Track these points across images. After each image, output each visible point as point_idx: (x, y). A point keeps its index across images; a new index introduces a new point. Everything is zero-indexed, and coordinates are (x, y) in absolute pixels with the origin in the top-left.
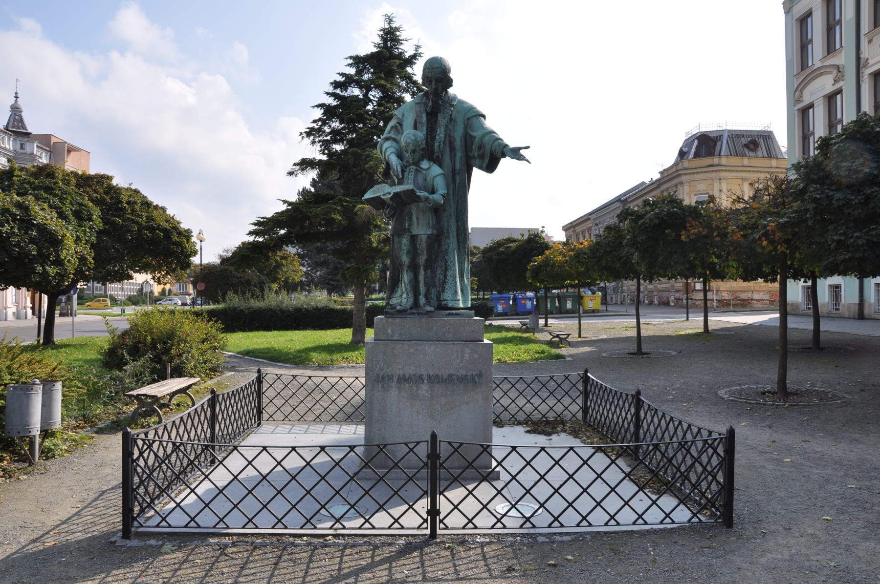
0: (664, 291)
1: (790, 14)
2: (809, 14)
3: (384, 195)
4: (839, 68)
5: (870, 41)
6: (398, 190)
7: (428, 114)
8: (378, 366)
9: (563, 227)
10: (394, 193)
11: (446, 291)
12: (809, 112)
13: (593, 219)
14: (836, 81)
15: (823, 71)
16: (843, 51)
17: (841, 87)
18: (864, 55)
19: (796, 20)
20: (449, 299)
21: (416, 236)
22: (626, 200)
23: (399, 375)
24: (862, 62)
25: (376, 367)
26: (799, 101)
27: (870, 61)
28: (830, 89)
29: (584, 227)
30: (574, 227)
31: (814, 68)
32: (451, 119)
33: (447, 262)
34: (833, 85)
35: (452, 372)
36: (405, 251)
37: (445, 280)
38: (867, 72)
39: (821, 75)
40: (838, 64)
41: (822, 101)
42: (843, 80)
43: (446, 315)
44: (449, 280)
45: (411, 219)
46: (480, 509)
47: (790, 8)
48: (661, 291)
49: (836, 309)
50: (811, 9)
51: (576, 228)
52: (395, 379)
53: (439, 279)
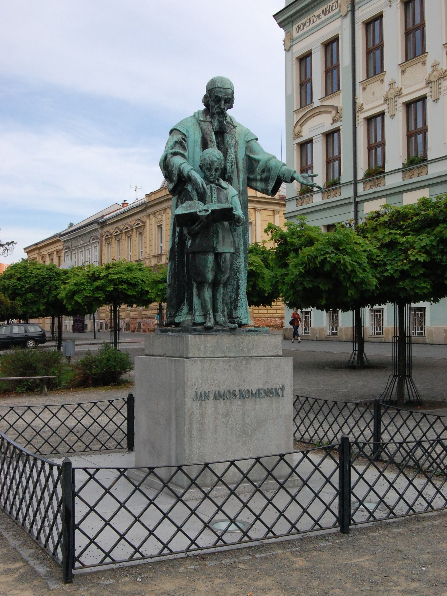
0: (149, 318)
1: (290, 52)
2: (309, 55)
3: (200, 211)
4: (337, 109)
5: (364, 89)
6: (216, 208)
7: (216, 133)
8: (196, 384)
9: (25, 249)
10: (212, 211)
11: (238, 308)
12: (307, 146)
13: (64, 241)
14: (334, 121)
15: (322, 109)
16: (341, 94)
17: (340, 127)
18: (360, 100)
19: (296, 58)
20: (242, 317)
21: (221, 254)
22: (104, 222)
23: (215, 392)
24: (358, 106)
25: (195, 384)
26: (298, 135)
27: (364, 106)
28: (328, 127)
29: (52, 249)
30: (39, 249)
31: (314, 107)
32: (236, 141)
33: (239, 280)
34: (332, 124)
35: (261, 386)
36: (210, 269)
37: (237, 298)
38: (361, 117)
39: (320, 113)
40: (336, 105)
41: (321, 138)
42: (341, 121)
43: (247, 331)
44: (241, 298)
45: (217, 237)
46: (173, 533)
47: (291, 47)
48: (146, 318)
49: (334, 333)
50: (311, 50)
51: (42, 251)
52: (212, 396)
53: (231, 297)
